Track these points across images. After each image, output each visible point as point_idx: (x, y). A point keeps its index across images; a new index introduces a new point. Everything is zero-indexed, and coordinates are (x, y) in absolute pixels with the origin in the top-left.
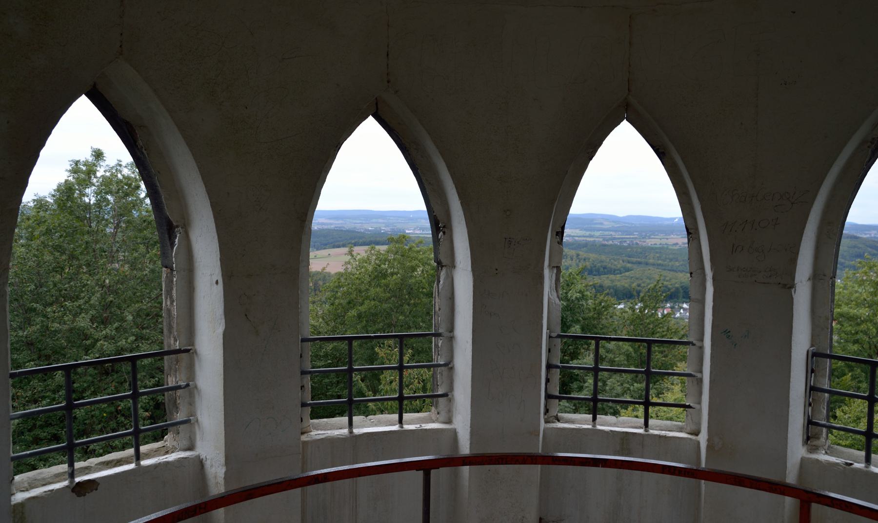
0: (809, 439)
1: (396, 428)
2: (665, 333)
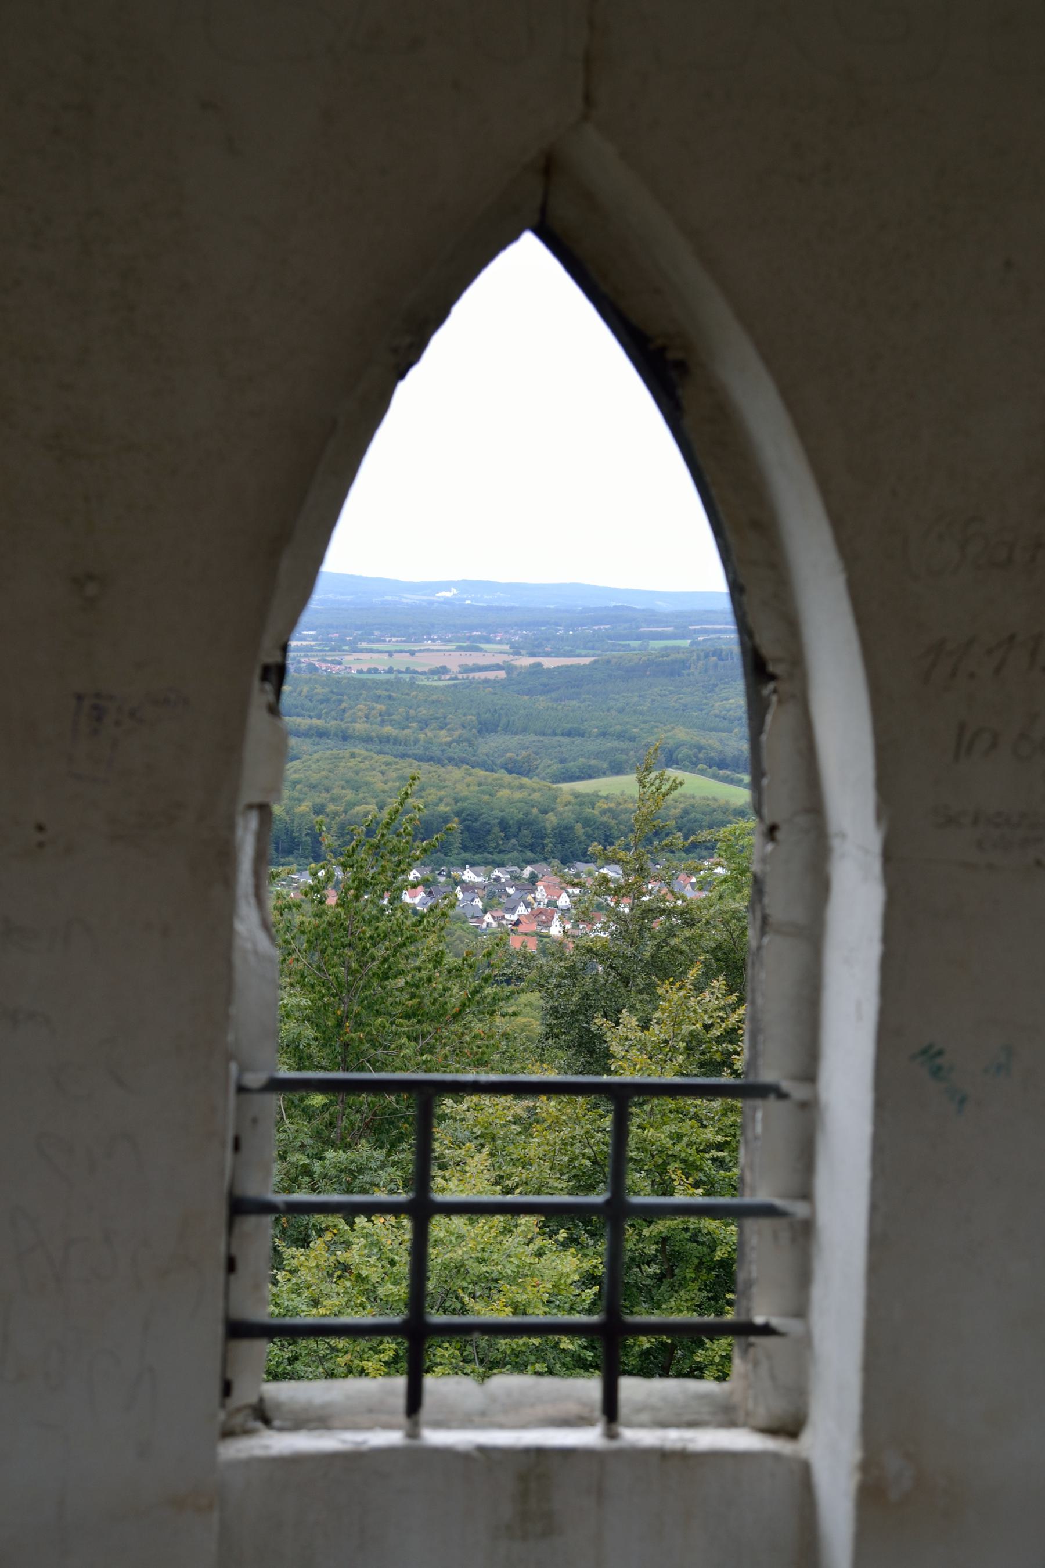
2: (424, 974)
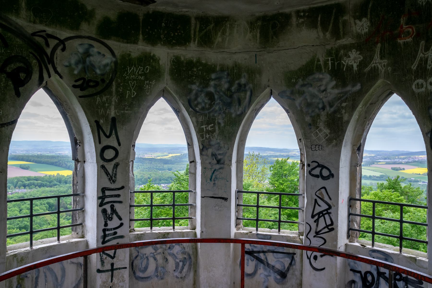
0: (237, 225)
1: (56, 243)
